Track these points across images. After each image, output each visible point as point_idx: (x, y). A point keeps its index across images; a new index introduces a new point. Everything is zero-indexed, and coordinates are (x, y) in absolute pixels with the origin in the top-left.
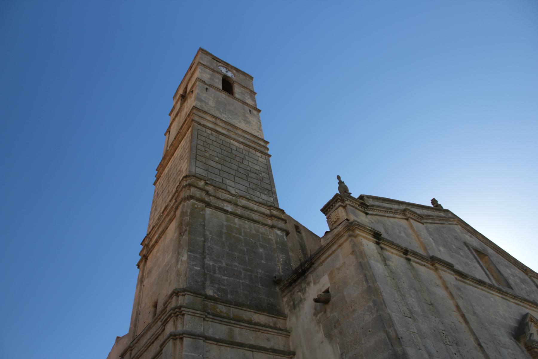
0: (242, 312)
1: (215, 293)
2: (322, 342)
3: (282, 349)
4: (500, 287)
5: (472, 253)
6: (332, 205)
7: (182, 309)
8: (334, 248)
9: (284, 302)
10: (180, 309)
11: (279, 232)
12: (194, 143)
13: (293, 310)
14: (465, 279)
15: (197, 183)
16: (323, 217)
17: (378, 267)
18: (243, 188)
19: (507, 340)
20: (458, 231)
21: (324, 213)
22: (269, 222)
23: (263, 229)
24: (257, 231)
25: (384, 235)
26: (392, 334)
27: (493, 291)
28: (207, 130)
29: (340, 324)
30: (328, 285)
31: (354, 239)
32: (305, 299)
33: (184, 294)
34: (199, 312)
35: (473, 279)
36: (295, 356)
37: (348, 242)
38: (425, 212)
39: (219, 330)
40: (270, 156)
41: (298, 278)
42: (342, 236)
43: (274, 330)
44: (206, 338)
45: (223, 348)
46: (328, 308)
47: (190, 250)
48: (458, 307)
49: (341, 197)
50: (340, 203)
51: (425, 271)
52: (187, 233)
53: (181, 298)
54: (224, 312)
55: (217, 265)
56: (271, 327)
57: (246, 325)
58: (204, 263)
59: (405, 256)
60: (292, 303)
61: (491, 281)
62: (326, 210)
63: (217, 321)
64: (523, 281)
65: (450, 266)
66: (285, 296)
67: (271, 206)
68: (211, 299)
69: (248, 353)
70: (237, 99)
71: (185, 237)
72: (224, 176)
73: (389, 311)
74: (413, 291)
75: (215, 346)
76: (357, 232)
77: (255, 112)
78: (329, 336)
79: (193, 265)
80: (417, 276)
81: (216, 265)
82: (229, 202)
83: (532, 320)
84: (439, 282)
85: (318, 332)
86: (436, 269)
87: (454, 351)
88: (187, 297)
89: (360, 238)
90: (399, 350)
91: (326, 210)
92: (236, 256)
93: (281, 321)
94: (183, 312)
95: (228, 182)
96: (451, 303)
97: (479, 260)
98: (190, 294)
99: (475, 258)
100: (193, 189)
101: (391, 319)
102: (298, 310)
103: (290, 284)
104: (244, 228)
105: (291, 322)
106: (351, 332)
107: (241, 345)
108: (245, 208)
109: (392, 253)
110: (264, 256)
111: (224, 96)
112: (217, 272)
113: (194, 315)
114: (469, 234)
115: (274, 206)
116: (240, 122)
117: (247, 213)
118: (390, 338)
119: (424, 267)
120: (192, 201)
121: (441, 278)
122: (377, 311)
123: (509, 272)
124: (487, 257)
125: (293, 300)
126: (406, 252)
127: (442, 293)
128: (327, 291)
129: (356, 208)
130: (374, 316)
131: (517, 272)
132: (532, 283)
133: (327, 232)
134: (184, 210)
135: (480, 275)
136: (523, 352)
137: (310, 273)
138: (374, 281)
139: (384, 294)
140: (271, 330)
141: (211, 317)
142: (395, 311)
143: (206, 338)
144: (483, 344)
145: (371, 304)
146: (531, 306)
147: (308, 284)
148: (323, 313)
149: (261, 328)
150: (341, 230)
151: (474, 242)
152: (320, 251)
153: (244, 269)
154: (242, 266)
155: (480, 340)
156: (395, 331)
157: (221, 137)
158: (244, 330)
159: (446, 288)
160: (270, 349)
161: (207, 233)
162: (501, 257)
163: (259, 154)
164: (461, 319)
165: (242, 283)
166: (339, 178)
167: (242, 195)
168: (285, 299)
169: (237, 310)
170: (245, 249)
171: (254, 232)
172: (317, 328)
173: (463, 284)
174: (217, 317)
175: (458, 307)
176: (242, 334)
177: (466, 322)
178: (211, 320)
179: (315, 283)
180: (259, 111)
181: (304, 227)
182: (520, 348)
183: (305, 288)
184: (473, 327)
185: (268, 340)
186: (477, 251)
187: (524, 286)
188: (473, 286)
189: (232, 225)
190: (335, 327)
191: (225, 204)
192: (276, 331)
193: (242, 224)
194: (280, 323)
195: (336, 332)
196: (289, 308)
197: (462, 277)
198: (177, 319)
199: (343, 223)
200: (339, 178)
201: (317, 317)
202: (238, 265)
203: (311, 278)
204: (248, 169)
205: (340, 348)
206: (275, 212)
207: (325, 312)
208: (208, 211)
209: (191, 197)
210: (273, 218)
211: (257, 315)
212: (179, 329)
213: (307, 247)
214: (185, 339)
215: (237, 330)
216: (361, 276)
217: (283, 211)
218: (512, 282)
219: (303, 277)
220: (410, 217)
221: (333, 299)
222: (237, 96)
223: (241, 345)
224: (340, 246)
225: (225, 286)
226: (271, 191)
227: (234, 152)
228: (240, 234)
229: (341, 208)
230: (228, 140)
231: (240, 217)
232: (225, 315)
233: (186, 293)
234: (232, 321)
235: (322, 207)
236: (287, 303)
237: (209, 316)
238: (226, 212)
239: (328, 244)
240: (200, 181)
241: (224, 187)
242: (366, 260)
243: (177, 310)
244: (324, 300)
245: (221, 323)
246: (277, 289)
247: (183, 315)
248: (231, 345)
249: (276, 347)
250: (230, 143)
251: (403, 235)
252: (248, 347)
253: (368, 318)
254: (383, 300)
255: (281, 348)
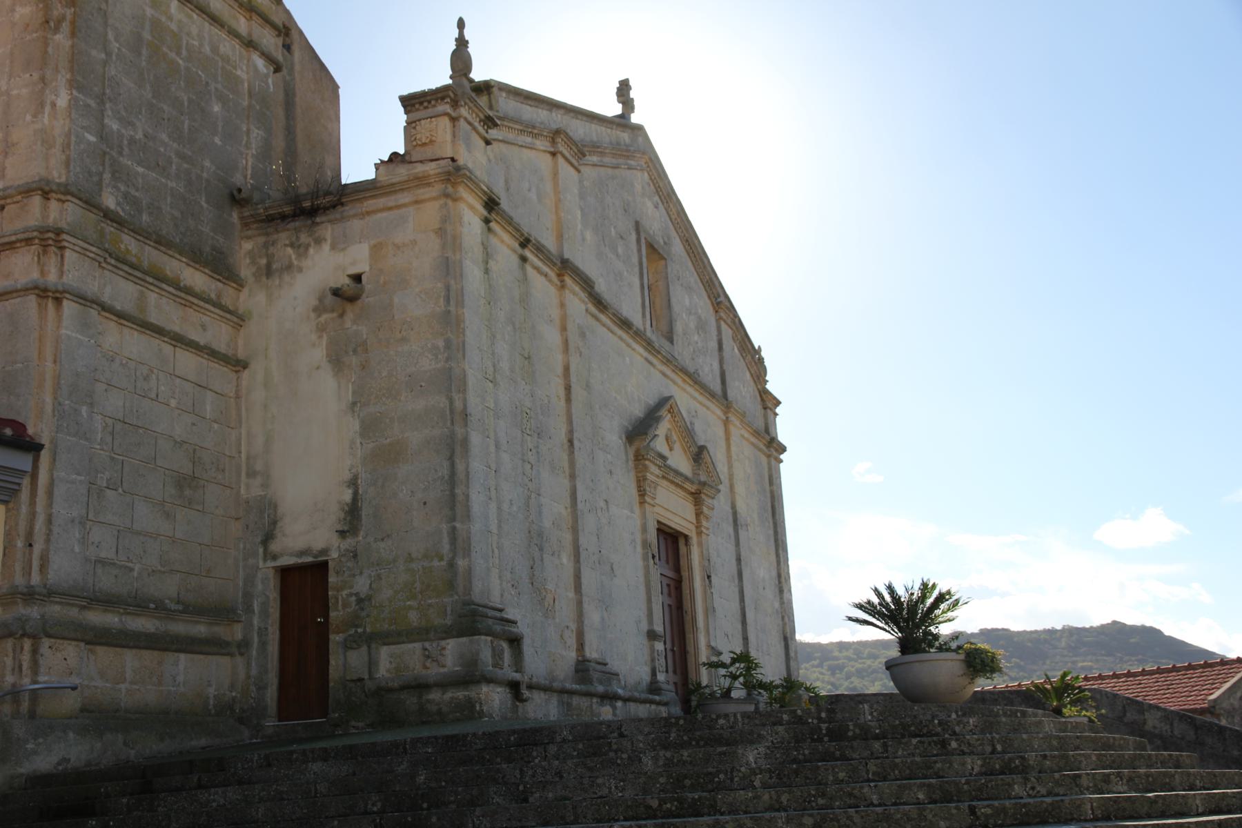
0: (166, 258)
1: (118, 204)
3: (223, 351)
4: (654, 338)
5: (639, 250)
6: (429, 102)
7: (64, 236)
10: (58, 234)
11: (260, 63)
13: (264, 279)
14: (601, 311)
16: (400, 118)
17: (473, 273)
19: (614, 438)
20: (638, 187)
21: (404, 106)
23: (229, 47)
25: (504, 204)
26: (458, 405)
27: (638, 342)
29: (366, 351)
31: (450, 202)
33: (63, 197)
34: (94, 249)
35: (614, 315)
36: (246, 371)
37: (437, 204)
39: (122, 292)
41: (295, 216)
42: (429, 185)
43: (217, 311)
44: (104, 308)
45: (126, 331)
46: (351, 311)
47: (73, 84)
48: (567, 369)
49: (456, 95)
51: (542, 286)
52: (66, 26)
53: (54, 205)
55: (128, 132)
56: (208, 301)
57: (171, 289)
58: (103, 126)
60: (264, 261)
61: (644, 325)
62: (411, 102)
63: (121, 273)
65: (587, 284)
66: (249, 238)
68: (112, 220)
69: (167, 349)
71: (61, 39)
73: (467, 367)
74: (509, 328)
75: (112, 324)
78: (336, 361)
79: (83, 128)
81: (123, 131)
84: (555, 313)
86: (563, 286)
87: (530, 446)
88: (69, 206)
90: (459, 431)
91: (411, 102)
92: (165, 116)
93: (231, 291)
94: (66, 244)
96: (559, 358)
97: (644, 260)
98: (77, 201)
102: (277, 282)
103: (270, 219)
104: (188, 34)
107: (158, 331)
109: (503, 241)
110: (220, 124)
112: (126, 151)
113: (83, 253)
114: (656, 198)
118: (452, 411)
119: (543, 278)
121: (562, 305)
122: (448, 359)
124: (663, 262)
126: (525, 243)
127: (552, 336)
128: (357, 278)
129: (474, 129)
130: (439, 366)
133: (395, 155)
136: (627, 461)
137: (329, 221)
138: (460, 303)
139: (468, 333)
140: (212, 309)
141: (113, 262)
142: (473, 368)
143: (104, 308)
144: (576, 443)
145: (441, 344)
146: (684, 381)
147: (319, 241)
148: (335, 315)
149: (196, 301)
150: (432, 172)
151: (655, 220)
152: (368, 190)
153: (178, 154)
154: (175, 145)
155: (575, 435)
158: (164, 300)
159: (564, 329)
161: (111, 36)
162: (690, 264)
164: (562, 392)
165: (172, 189)
166: (461, 24)
168: (248, 246)
169: (156, 252)
170: (186, 98)
172: (314, 337)
173: (594, 323)
175: (567, 369)
176: (163, 309)
177: (568, 400)
178: (110, 268)
179: (333, 247)
181: (301, 33)
182: (627, 455)
183: (307, 247)
184: (573, 411)
187: (696, 338)
189: (164, 19)
190: (355, 351)
192: (221, 313)
193: (185, 20)
194: (228, 295)
195: (354, 360)
196: (254, 269)
197: (597, 307)
198: (45, 252)
199: (441, 162)
200: (461, 24)
201: (319, 316)
202: (167, 140)
203: (328, 231)
205: (354, 393)
207: (342, 315)
210: (255, 17)
211: (191, 270)
212: (52, 278)
213: (297, 99)
214: (65, 302)
215: (152, 297)
216: (439, 285)
218: (679, 328)
219: (309, 222)
221: (366, 300)
223: (158, 331)
224: (417, 202)
225: (137, 190)
228: (179, 54)
229: (446, 120)
232: (134, 260)
233: (69, 198)
235: (405, 93)
236: (250, 253)
237: (109, 260)
239: (393, 184)
242: (458, 257)
244: (347, 295)
245: (128, 277)
246: (235, 216)
248: (141, 326)
249: (215, 346)
251: (533, 196)
252: (171, 339)
253: (427, 364)
254: (464, 343)
255: (221, 347)
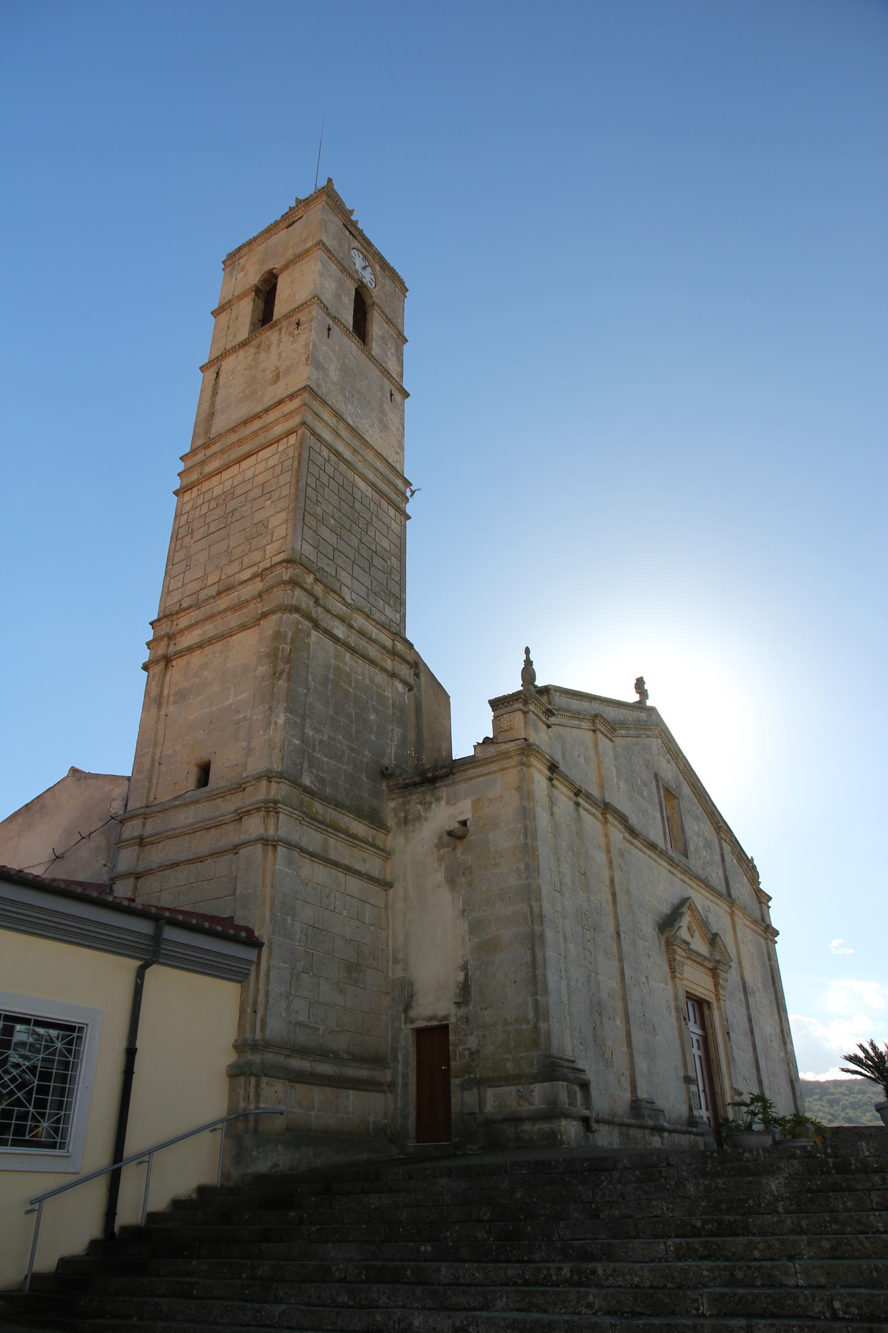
2: (439, 886)
5: (659, 793)
6: (508, 703)
7: (280, 805)
8: (494, 767)
9: (390, 807)
10: (275, 804)
11: (399, 686)
12: (302, 483)
13: (403, 826)
14: (634, 838)
15: (304, 579)
16: (490, 714)
18: (362, 591)
19: (649, 929)
22: (389, 664)
24: (372, 681)
25: (562, 767)
26: (536, 910)
28: (323, 447)
29: (471, 873)
30: (467, 816)
31: (525, 768)
32: (426, 819)
34: (297, 812)
37: (515, 770)
38: (622, 714)
39: (313, 839)
40: (409, 518)
41: (422, 783)
42: (510, 757)
43: (373, 849)
45: (316, 865)
47: (288, 710)
48: (612, 881)
50: (521, 706)
51: (591, 822)
52: (285, 676)
54: (321, 813)
57: (344, 836)
58: (304, 733)
59: (575, 798)
60: (402, 815)
61: (666, 845)
64: (708, 845)
65: (623, 819)
66: (393, 799)
67: (396, 634)
69: (341, 876)
70: (371, 357)
72: (339, 562)
73: (541, 883)
75: (307, 861)
76: (533, 761)
77: (398, 397)
78: (451, 882)
80: (580, 832)
82: (342, 620)
83: (693, 909)
84: (602, 841)
85: (436, 870)
86: (606, 822)
87: (589, 937)
88: (283, 786)
89: (533, 770)
90: (538, 929)
94: (280, 810)
95: (345, 577)
96: (606, 873)
97: (663, 799)
99: (660, 802)
100: (298, 592)
101: (539, 892)
103: (406, 786)
104: (356, 673)
105: (395, 840)
106: (484, 889)
107: (335, 864)
108: (362, 633)
111: (352, 346)
112: (317, 748)
114: (669, 756)
115: (398, 634)
116: (372, 426)
117: (362, 643)
118: (532, 915)
119: (592, 817)
120: (296, 615)
121: (607, 835)
122: (528, 877)
123: (696, 828)
124: (676, 801)
125: (407, 812)
126: (578, 793)
127: (600, 857)
128: (464, 823)
129: (539, 718)
130: (521, 882)
131: (708, 830)
132: (717, 848)
134: (282, 630)
135: (656, 832)
136: (660, 947)
138: (535, 838)
139: (541, 858)
141: (308, 820)
144: (622, 934)
145: (522, 867)
146: (698, 885)
147: (438, 799)
148: (450, 849)
149: (359, 843)
151: (669, 771)
155: (621, 929)
156: (541, 907)
157: (342, 467)
159: (608, 852)
160: (366, 874)
161: (310, 679)
163: (392, 512)
164: (609, 898)
166: (527, 651)
167: (359, 605)
168: (392, 805)
171: (367, 681)
174: (314, 820)
175: (612, 881)
176: (339, 850)
177: (615, 903)
179: (447, 803)
180: (406, 395)
182: (660, 942)
183: (430, 803)
185: (364, 860)
186: (667, 790)
187: (705, 853)
188: (640, 850)
189: (341, 665)
190: (463, 874)
191: (336, 624)
194: (381, 839)
197: (632, 836)
200: (527, 651)
203: (444, 792)
204: (374, 547)
205: (464, 903)
206: (399, 646)
207: (454, 849)
208: (315, 635)
209: (296, 609)
210: (397, 658)
213: (423, 707)
214: (279, 848)
215: (332, 842)
216: (520, 825)
217: (411, 646)
218: (691, 847)
220: (599, 730)
221: (470, 838)
222: (376, 348)
223: (335, 864)
224: (502, 769)
226: (399, 602)
227: (358, 505)
230: (350, 474)
231: (353, 651)
232: (321, 818)
234: (329, 830)
236: (395, 811)
238: (336, 639)
240: (308, 575)
241: (336, 586)
242: (532, 805)
243: (271, 805)
244: (457, 835)
247: (278, 813)
249: (371, 873)
250: (354, 485)
251: (582, 760)
255: (376, 874)
